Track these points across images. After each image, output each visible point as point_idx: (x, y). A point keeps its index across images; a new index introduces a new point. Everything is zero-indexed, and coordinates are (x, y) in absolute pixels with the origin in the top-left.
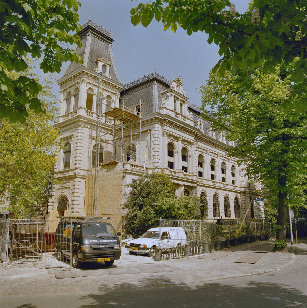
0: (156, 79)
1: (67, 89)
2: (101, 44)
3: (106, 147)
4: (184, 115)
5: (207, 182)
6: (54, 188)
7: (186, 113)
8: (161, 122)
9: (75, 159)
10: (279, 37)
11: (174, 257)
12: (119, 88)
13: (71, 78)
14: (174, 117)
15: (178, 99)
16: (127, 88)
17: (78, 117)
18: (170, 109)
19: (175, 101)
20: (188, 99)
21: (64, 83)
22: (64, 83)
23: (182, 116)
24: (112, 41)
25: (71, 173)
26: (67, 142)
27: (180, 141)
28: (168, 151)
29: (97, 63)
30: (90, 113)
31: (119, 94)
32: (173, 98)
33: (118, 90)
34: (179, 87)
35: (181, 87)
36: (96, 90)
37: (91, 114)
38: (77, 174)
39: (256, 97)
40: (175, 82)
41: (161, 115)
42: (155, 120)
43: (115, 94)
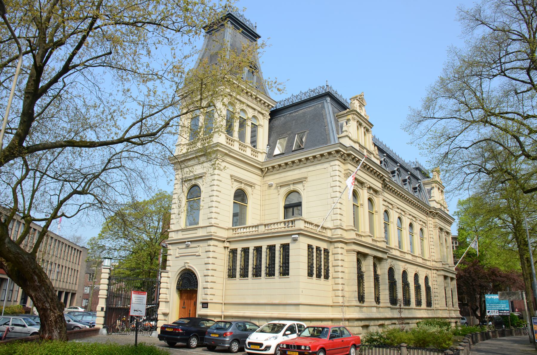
0: (328, 94)
2: (244, 42)
3: (252, 194)
8: (343, 157)
9: (209, 210)
12: (269, 105)
16: (279, 106)
17: (217, 144)
20: (373, 125)
25: (201, 233)
26: (194, 183)
27: (366, 189)
30: (231, 140)
31: (268, 114)
33: (267, 109)
35: (363, 108)
37: (232, 141)
38: (213, 234)
39: (498, 123)
40: (357, 100)
41: (345, 148)
42: (336, 155)
43: (262, 114)
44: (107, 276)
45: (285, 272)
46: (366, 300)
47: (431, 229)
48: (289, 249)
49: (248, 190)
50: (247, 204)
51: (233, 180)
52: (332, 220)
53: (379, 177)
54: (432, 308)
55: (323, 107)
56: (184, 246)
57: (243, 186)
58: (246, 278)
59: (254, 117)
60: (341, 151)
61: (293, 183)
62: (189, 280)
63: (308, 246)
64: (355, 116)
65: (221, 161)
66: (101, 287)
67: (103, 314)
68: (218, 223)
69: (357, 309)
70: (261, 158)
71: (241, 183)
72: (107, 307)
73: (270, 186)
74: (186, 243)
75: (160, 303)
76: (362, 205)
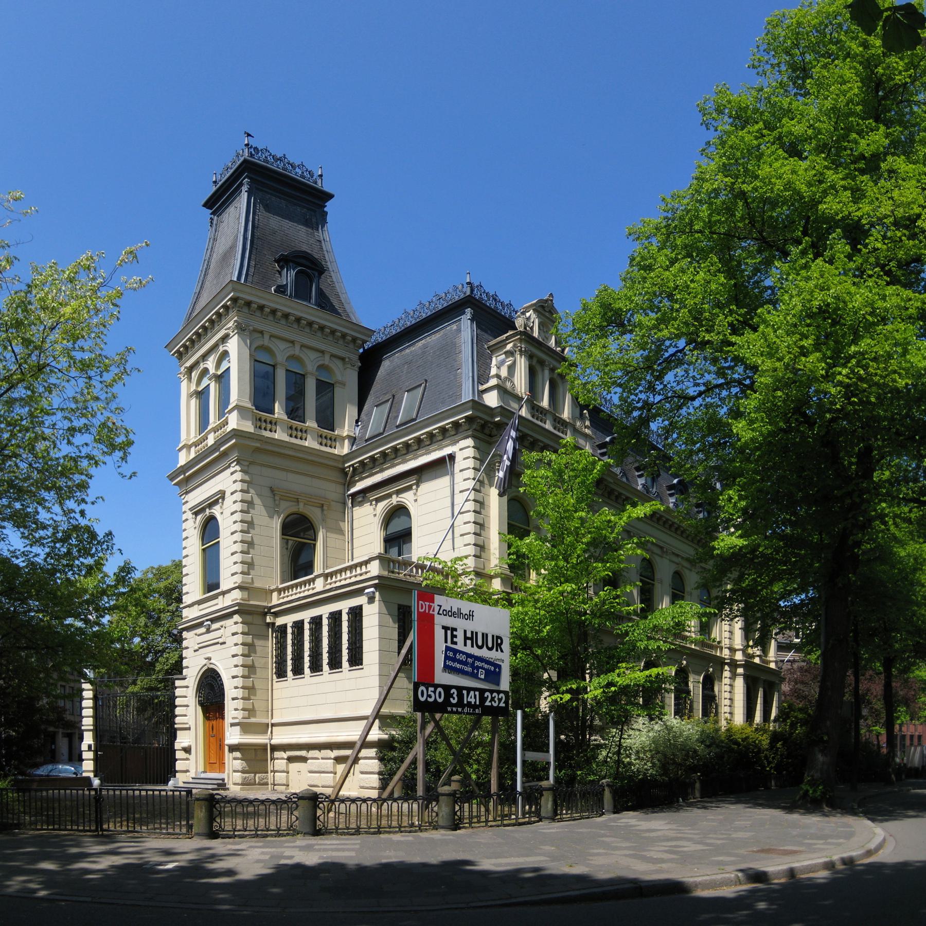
6: (187, 648)
8: (487, 431)
10: (606, 789)
15: (542, 363)
28: (508, 524)
36: (281, 351)
45: (356, 659)
48: (361, 616)
53: (667, 526)
55: (459, 330)
56: (203, 630)
57: (302, 508)
59: (322, 367)
62: (211, 687)
63: (399, 609)
72: (96, 745)
75: (178, 732)
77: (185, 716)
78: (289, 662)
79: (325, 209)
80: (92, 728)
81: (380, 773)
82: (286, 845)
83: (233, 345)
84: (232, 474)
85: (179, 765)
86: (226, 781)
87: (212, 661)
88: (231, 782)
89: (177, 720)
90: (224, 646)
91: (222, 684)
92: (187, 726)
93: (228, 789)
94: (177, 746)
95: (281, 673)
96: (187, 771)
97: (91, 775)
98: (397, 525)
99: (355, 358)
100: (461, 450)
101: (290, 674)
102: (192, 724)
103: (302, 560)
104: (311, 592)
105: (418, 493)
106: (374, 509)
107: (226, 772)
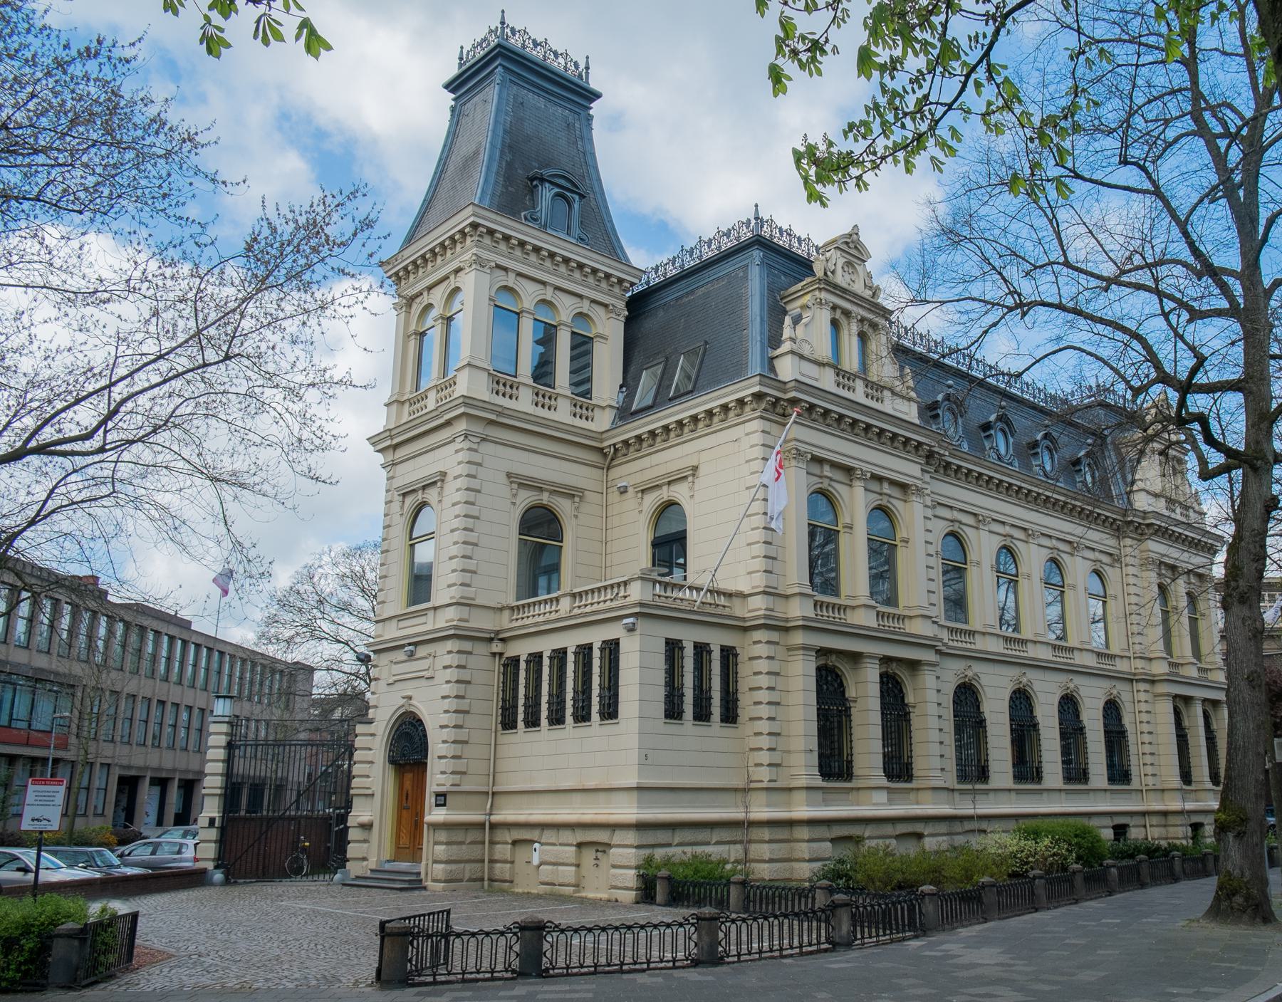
0: (760, 242)
1: (446, 278)
3: (576, 517)
4: (873, 378)
5: (981, 644)
7: (885, 369)
8: (779, 410)
11: (863, 938)
13: (442, 245)
14: (834, 389)
18: (816, 356)
19: (835, 324)
21: (417, 267)
22: (426, 261)
23: (868, 384)
24: (592, 101)
29: (532, 191)
30: (509, 384)
32: (825, 316)
34: (853, 267)
44: (222, 740)
45: (610, 711)
46: (856, 771)
47: (1131, 570)
49: (564, 507)
50: (562, 541)
51: (515, 486)
52: (748, 573)
54: (1135, 783)
56: (400, 655)
57: (545, 498)
58: (538, 729)
59: (581, 315)
60: (766, 395)
61: (669, 483)
64: (824, 295)
65: (479, 440)
66: (209, 768)
67: (213, 834)
68: (473, 596)
69: (1179, 795)
70: (602, 421)
71: (541, 489)
73: (621, 493)
74: (406, 649)
75: (355, 800)
76: (850, 527)
77: (368, 776)
78: (521, 709)
79: (591, 112)
80: (219, 791)
81: (637, 889)
82: (501, 993)
83: (470, 282)
84: (457, 451)
85: (352, 850)
86: (423, 876)
87: (412, 702)
88: (429, 878)
89: (355, 783)
90: (430, 682)
91: (425, 736)
92: (369, 792)
93: (425, 888)
94: (351, 822)
95: (508, 723)
96: (364, 859)
97: (210, 866)
98: (669, 528)
99: (621, 305)
100: (747, 434)
101: (521, 724)
102: (376, 789)
103: (546, 561)
104: (554, 616)
105: (696, 487)
106: (640, 504)
107: (424, 862)
